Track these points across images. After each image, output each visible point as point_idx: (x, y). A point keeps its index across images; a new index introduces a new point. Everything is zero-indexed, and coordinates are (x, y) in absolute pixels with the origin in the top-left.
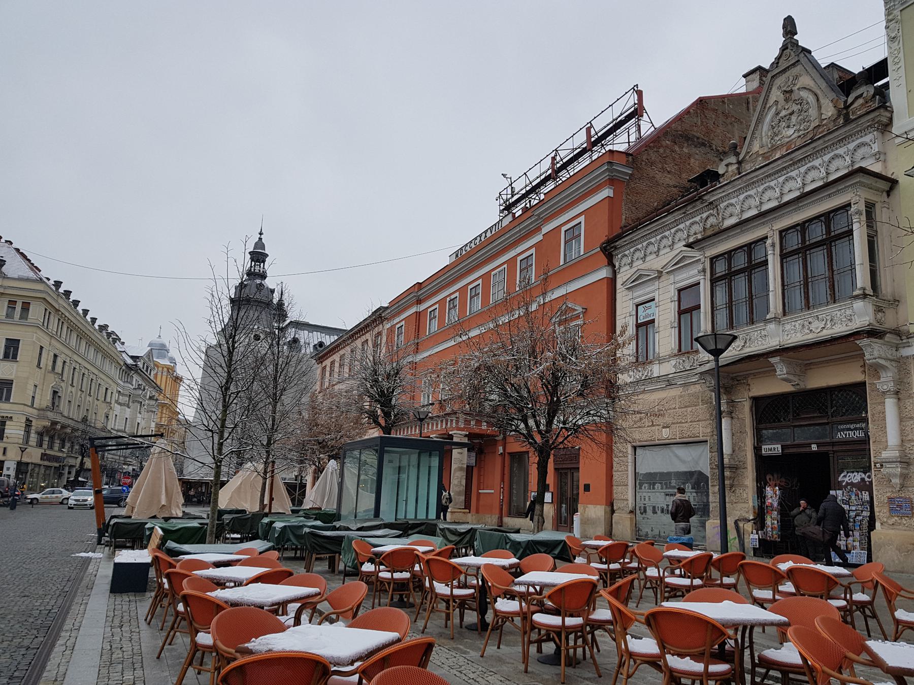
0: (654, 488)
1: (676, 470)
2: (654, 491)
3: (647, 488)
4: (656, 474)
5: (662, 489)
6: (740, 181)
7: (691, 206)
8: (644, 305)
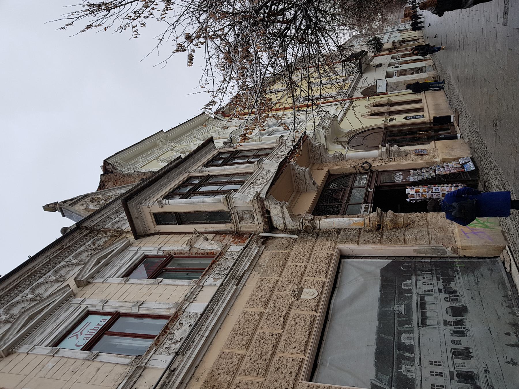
0: (410, 348)
1: (376, 304)
2: (417, 350)
3: (409, 367)
4: (380, 341)
5: (411, 332)
6: (115, 205)
7: (68, 239)
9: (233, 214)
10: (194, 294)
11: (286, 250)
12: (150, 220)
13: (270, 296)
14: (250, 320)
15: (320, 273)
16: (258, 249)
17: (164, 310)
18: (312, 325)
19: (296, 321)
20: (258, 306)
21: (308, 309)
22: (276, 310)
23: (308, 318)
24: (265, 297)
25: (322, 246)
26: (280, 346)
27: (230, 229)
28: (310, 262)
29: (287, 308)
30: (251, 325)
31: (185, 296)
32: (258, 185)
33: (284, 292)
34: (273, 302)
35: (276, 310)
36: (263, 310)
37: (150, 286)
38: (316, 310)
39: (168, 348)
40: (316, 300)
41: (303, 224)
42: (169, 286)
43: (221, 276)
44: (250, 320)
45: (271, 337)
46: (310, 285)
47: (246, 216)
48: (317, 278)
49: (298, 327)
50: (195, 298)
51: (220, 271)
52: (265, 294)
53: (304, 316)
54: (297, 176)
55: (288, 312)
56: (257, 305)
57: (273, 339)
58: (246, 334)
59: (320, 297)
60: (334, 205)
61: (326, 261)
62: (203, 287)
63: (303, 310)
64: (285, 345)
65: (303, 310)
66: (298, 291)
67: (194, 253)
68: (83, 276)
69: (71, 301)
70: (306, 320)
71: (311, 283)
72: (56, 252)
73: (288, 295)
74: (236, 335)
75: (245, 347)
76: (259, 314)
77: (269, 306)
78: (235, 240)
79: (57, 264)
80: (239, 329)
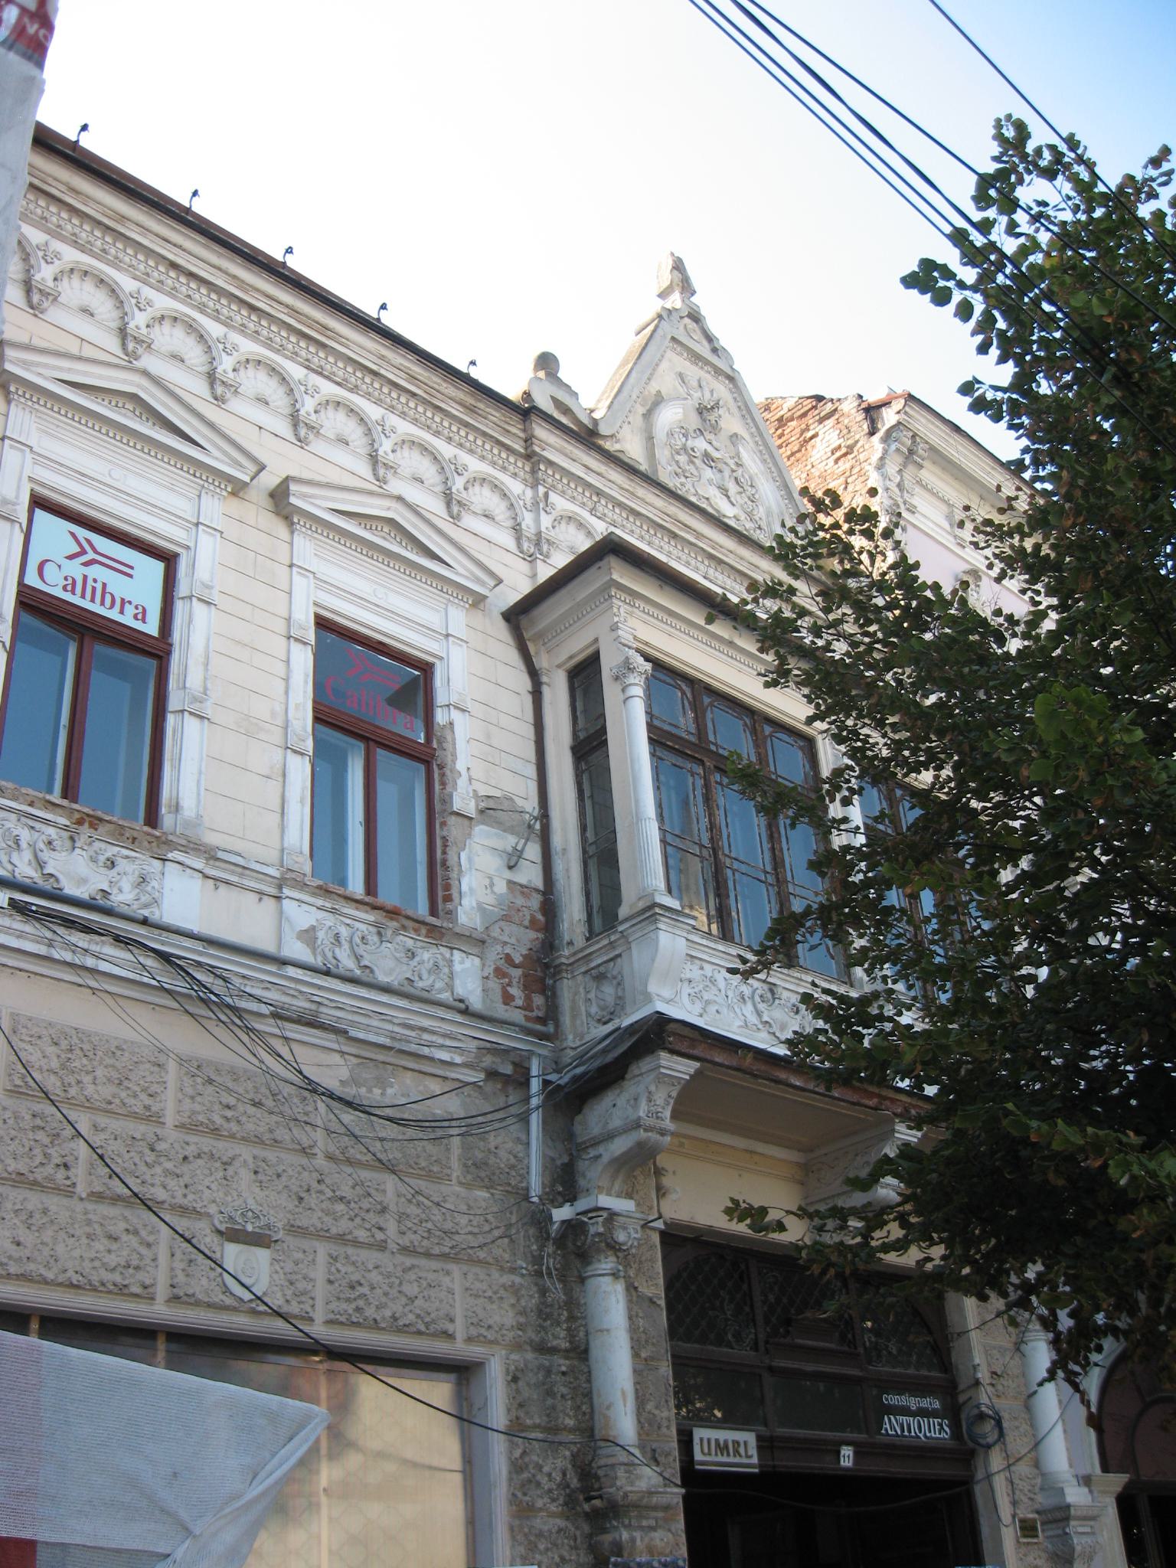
7: (470, 400)
8: (82, 533)
9: (605, 942)
10: (241, 875)
11: (465, 1165)
12: (575, 646)
13: (232, 1136)
14: (126, 1083)
15: (348, 1300)
16: (458, 1060)
18: (110, 1292)
19: (125, 1237)
20: (187, 1100)
23: (141, 1276)
24: (228, 1119)
25: (489, 1293)
26: (28, 1194)
28: (400, 1258)
29: (180, 1200)
30: (106, 1091)
31: (229, 847)
32: (759, 1014)
33: (255, 1181)
34: (206, 1150)
36: (170, 1119)
37: (280, 722)
39: (19, 846)
41: (590, 1215)
43: (327, 950)
45: (58, 1161)
46: (287, 1270)
47: (609, 990)
49: (101, 1245)
50: (227, 883)
51: (351, 942)
53: (148, 1261)
54: (859, 1158)
55: (166, 1206)
57: (49, 1170)
58: (71, 1079)
59: (235, 1309)
62: (278, 898)
63: (173, 1255)
64: (24, 1212)
65: (173, 1255)
66: (257, 1230)
69: (210, 494)
71: (295, 1273)
72: (413, 378)
73: (239, 1196)
74: (63, 1047)
75: (16, 1086)
76: (153, 1109)
78: (516, 966)
79: (368, 395)
80: (90, 1054)
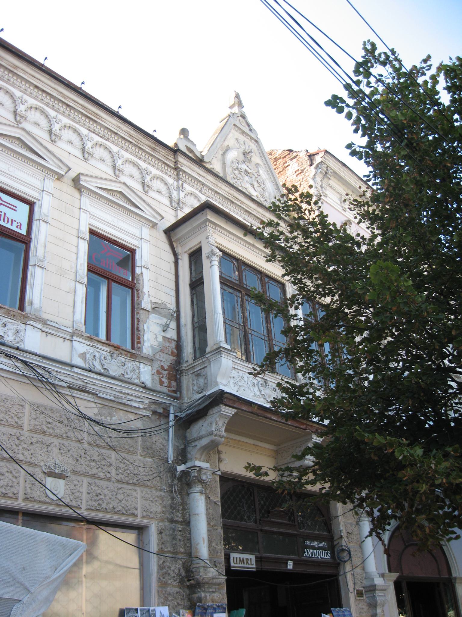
7: (153, 146)
9: (201, 361)
10: (57, 331)
12: (192, 245)
13: (51, 435)
14: (8, 413)
16: (141, 406)
17: (31, 298)
19: (7, 474)
21: (28, 488)
22: (25, 446)
24: (49, 428)
25: (151, 499)
27: (185, 360)
28: (116, 484)
32: (260, 391)
35: (25, 446)
36: (26, 427)
37: (74, 270)
38: (26, 499)
40: (45, 498)
42: (73, 296)
43: (90, 362)
44: (8, 413)
46: (72, 488)
47: (201, 381)
48: (84, 496)
52: (55, 428)
54: (298, 449)
56: (35, 419)
59: (50, 504)
60: (255, 511)
61: (120, 507)
62: (71, 341)
67: (138, 317)
68: (85, 181)
70: (9, 487)
72: (131, 136)
73: (53, 458)
77: (33, 435)
79: (113, 142)
